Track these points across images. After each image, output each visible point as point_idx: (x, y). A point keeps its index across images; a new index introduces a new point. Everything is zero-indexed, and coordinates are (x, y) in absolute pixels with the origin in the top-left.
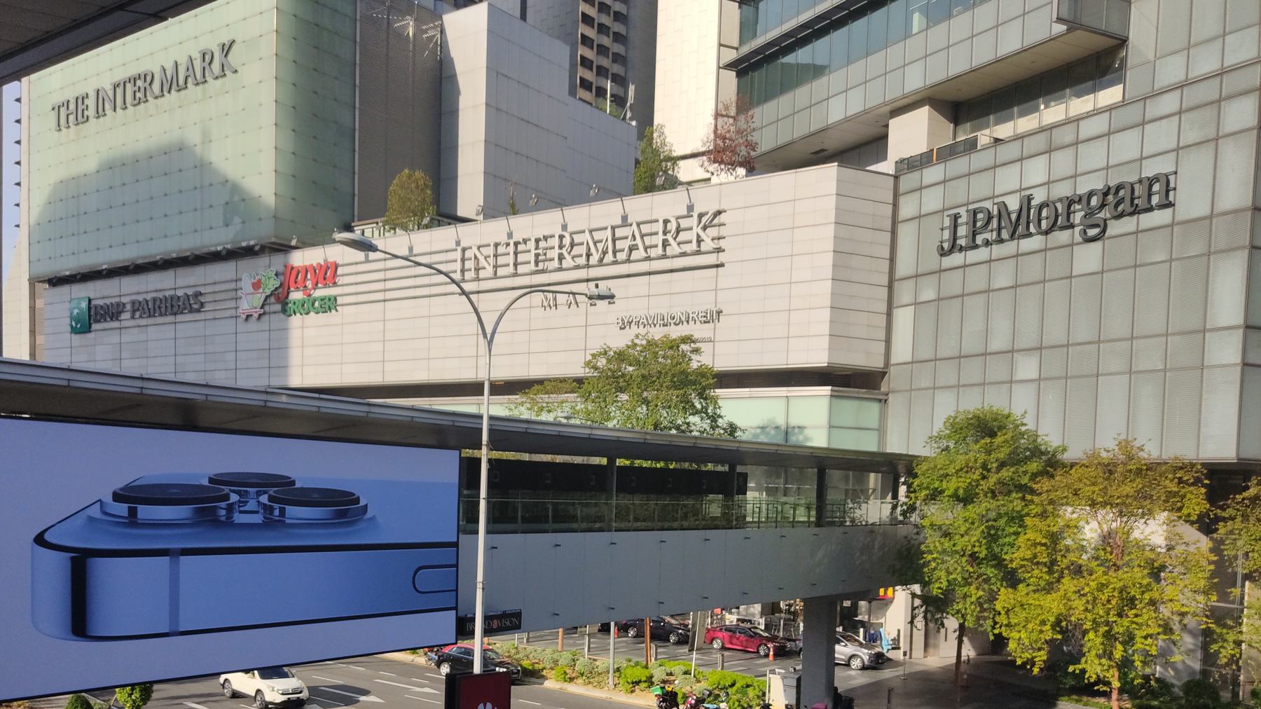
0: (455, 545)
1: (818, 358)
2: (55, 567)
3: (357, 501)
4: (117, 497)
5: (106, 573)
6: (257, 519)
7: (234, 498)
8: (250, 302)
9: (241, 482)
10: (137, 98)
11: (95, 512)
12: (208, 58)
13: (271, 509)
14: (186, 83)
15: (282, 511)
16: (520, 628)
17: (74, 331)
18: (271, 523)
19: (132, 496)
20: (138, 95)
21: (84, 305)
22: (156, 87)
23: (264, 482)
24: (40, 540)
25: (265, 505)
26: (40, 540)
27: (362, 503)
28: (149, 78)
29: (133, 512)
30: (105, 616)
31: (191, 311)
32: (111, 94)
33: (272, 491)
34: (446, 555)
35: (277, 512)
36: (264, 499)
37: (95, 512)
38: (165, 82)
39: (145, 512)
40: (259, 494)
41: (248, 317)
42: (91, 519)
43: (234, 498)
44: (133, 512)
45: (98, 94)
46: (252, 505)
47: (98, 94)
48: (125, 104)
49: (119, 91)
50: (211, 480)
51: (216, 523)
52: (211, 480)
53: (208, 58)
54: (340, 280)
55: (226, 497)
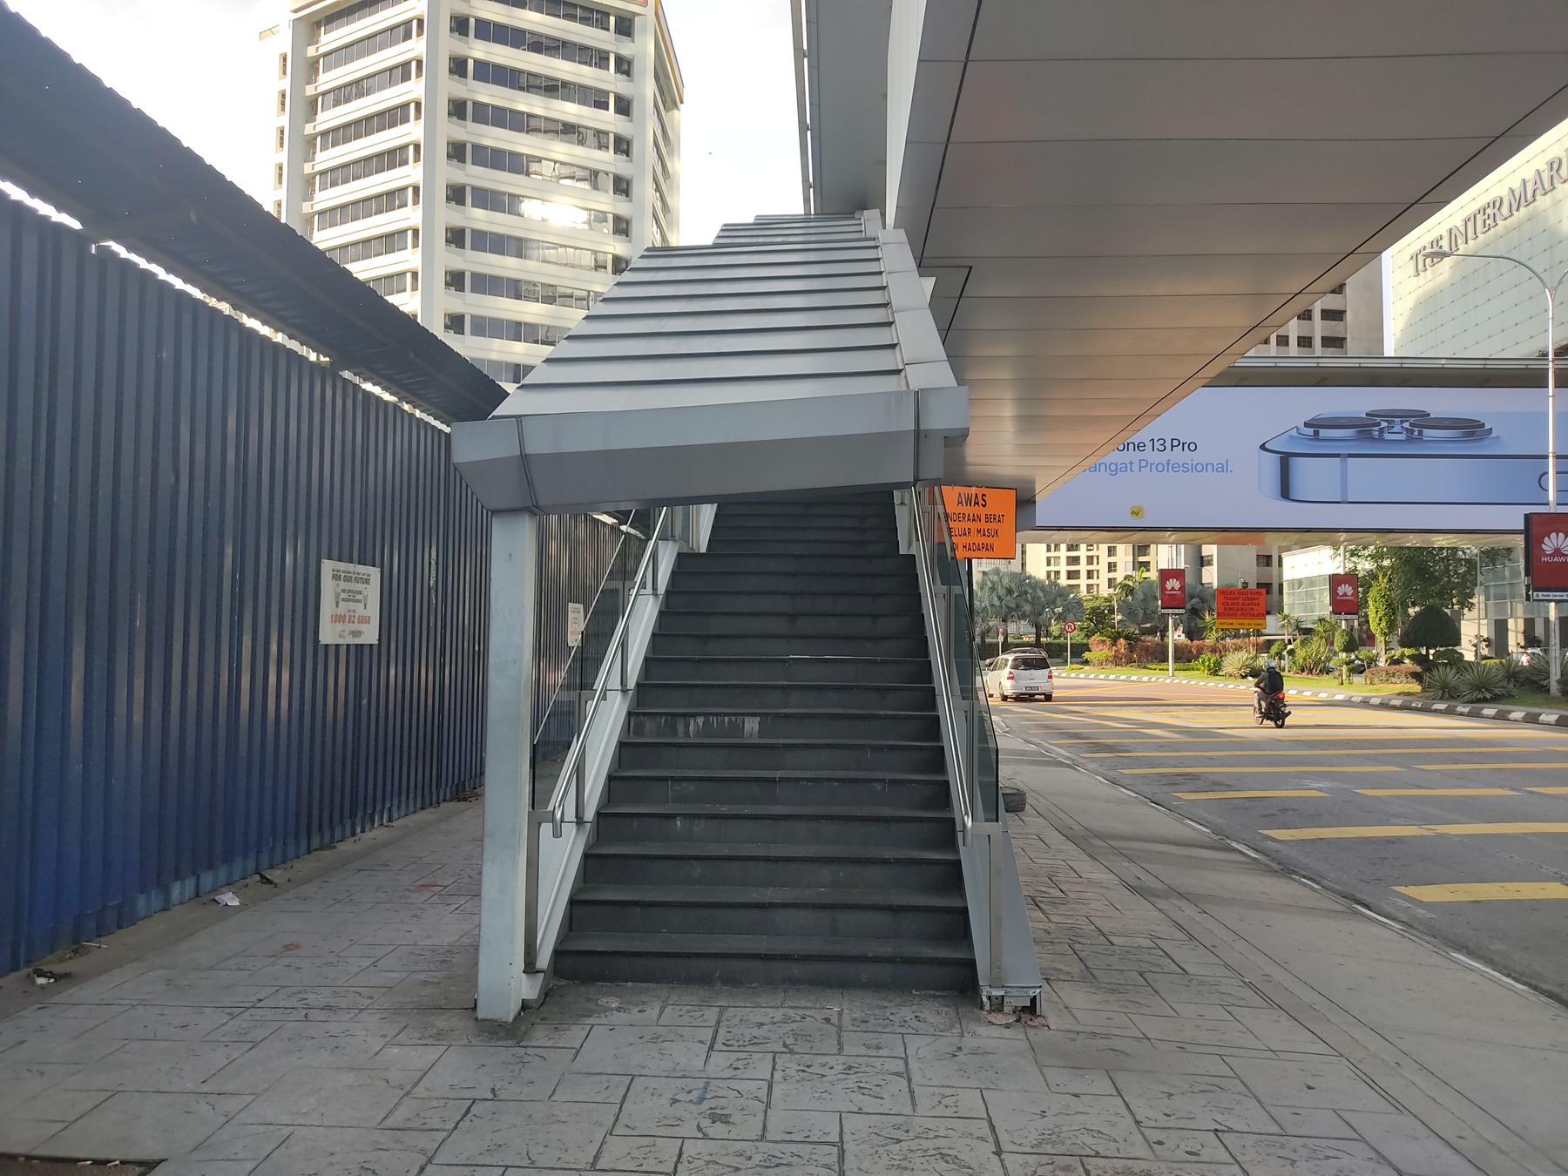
2: (1272, 462)
3: (1483, 425)
4: (1306, 425)
5: (1300, 466)
6: (1402, 437)
7: (1384, 424)
9: (1390, 415)
10: (1487, 225)
11: (1294, 433)
12: (1555, 166)
13: (1412, 431)
14: (1534, 196)
15: (1421, 433)
16: (1311, 338)
18: (1410, 440)
19: (1315, 425)
20: (1488, 222)
22: (1505, 210)
23: (1405, 415)
24: (1263, 447)
25: (1407, 428)
26: (1263, 447)
27: (1487, 427)
28: (1497, 205)
29: (1316, 433)
30: (1300, 487)
32: (1462, 229)
33: (1412, 420)
35: (1416, 433)
36: (1406, 425)
37: (1294, 433)
38: (1513, 202)
39: (1323, 433)
40: (1402, 422)
42: (1291, 436)
43: (1384, 424)
44: (1316, 433)
45: (1451, 233)
47: (1451, 233)
48: (1475, 234)
49: (1470, 225)
50: (1367, 414)
52: (1367, 414)
53: (1555, 166)
55: (1379, 424)
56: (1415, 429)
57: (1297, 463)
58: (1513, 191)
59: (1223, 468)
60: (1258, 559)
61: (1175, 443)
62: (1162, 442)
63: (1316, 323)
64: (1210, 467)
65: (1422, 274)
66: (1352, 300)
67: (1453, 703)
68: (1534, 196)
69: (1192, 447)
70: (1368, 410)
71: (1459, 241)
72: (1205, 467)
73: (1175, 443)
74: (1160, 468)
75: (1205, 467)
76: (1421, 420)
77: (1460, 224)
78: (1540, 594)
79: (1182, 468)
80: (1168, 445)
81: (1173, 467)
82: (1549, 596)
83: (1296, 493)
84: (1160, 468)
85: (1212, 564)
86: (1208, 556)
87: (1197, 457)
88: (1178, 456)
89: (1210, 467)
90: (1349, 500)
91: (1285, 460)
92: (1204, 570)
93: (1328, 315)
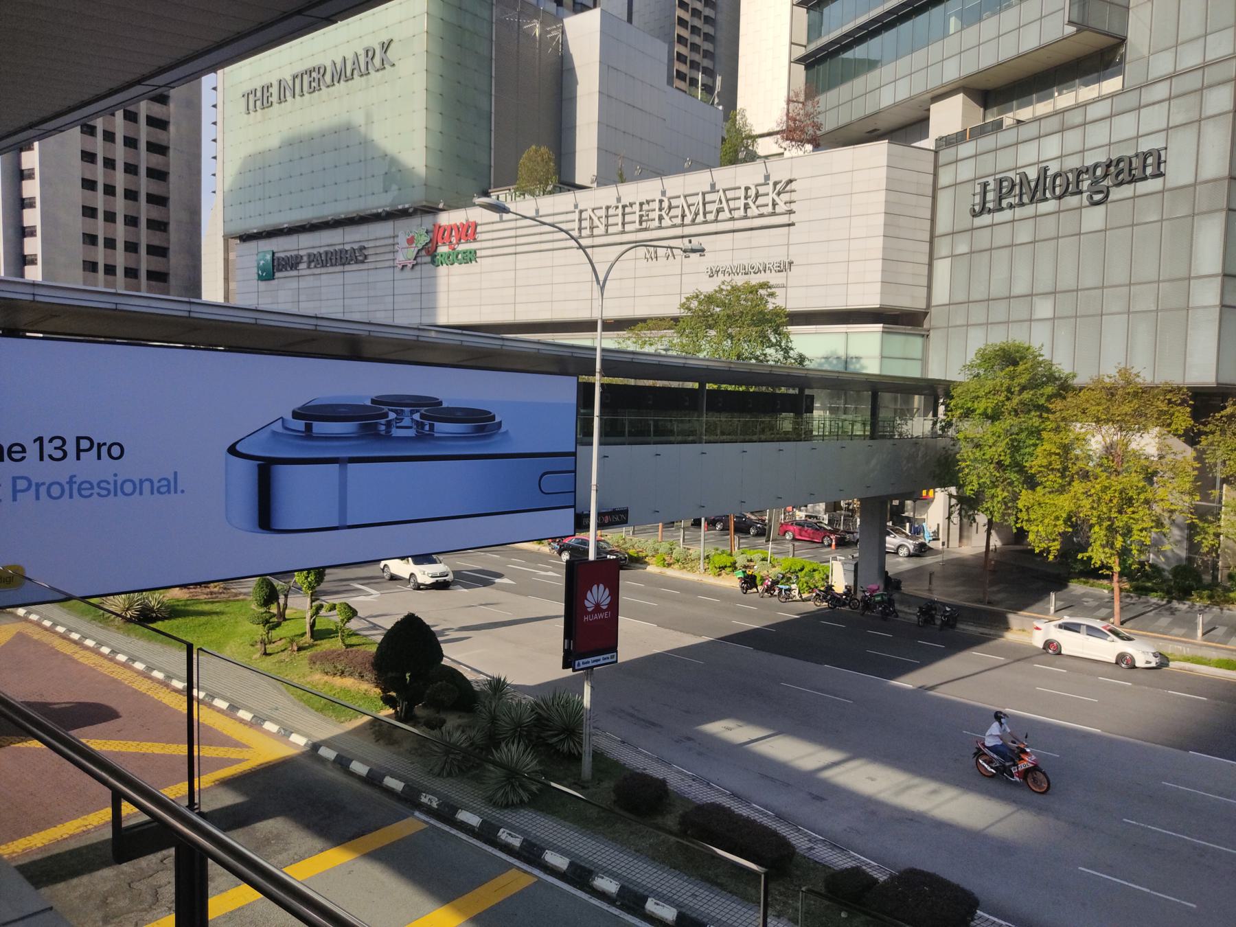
0: (574, 454)
1: (871, 299)
2: (245, 472)
3: (493, 418)
4: (296, 415)
6: (411, 433)
7: (392, 416)
8: (406, 254)
11: (278, 427)
12: (370, 54)
13: (423, 425)
14: (352, 75)
15: (432, 427)
17: (261, 278)
18: (421, 437)
19: (307, 414)
20: (313, 84)
21: (269, 257)
22: (328, 78)
24: (232, 450)
25: (417, 421)
26: (232, 450)
27: (497, 420)
29: (309, 428)
31: (357, 262)
33: (423, 410)
34: (566, 463)
35: (427, 428)
36: (417, 416)
37: (278, 427)
38: (335, 73)
39: (319, 427)
40: (412, 412)
41: (404, 267)
42: (274, 433)
43: (392, 416)
44: (309, 428)
45: (280, 84)
46: (406, 421)
47: (280, 84)
49: (298, 81)
50: (373, 401)
51: (377, 436)
52: (373, 401)
53: (370, 54)
54: (479, 237)
55: (386, 415)
56: (426, 422)
57: (283, 474)
58: (335, 64)
59: (169, 486)
60: (84, 264)
61: (85, 444)
62: (58, 443)
63: (141, 127)
64: (147, 485)
65: (252, 113)
66: (173, 111)
67: (497, 814)
68: (352, 75)
69: (116, 451)
70: (376, 393)
71: (288, 93)
72: (138, 487)
73: (85, 444)
74: (56, 491)
75: (138, 487)
76: (432, 410)
77: (289, 79)
78: (581, 661)
79: (96, 490)
80: (71, 448)
81: (79, 490)
82: (588, 662)
83: (283, 518)
84: (56, 491)
85: (35, 207)
86: (30, 198)
87: (126, 469)
88: (90, 467)
89: (147, 485)
90: (349, 524)
91: (266, 469)
92: (25, 183)
93: (153, 122)
